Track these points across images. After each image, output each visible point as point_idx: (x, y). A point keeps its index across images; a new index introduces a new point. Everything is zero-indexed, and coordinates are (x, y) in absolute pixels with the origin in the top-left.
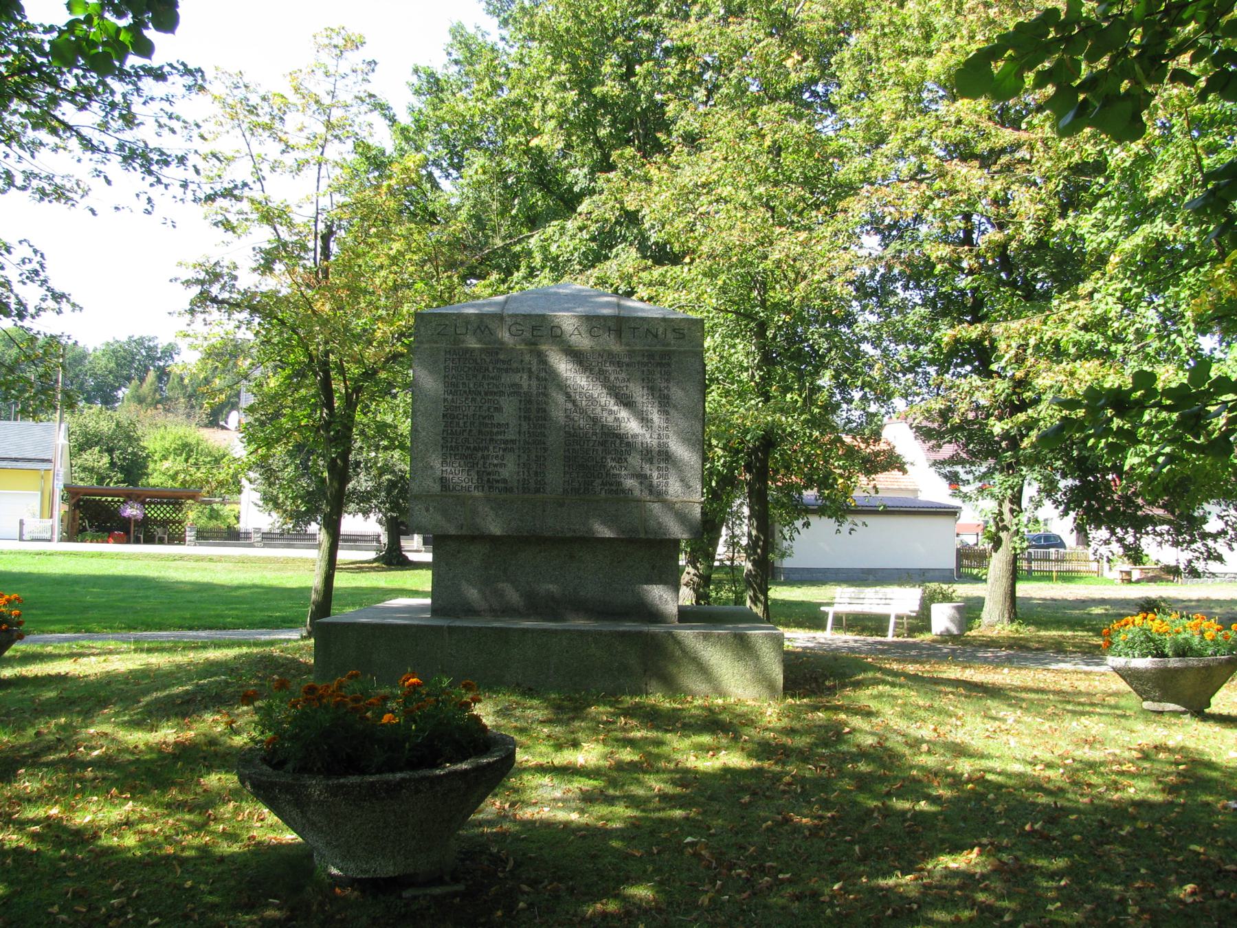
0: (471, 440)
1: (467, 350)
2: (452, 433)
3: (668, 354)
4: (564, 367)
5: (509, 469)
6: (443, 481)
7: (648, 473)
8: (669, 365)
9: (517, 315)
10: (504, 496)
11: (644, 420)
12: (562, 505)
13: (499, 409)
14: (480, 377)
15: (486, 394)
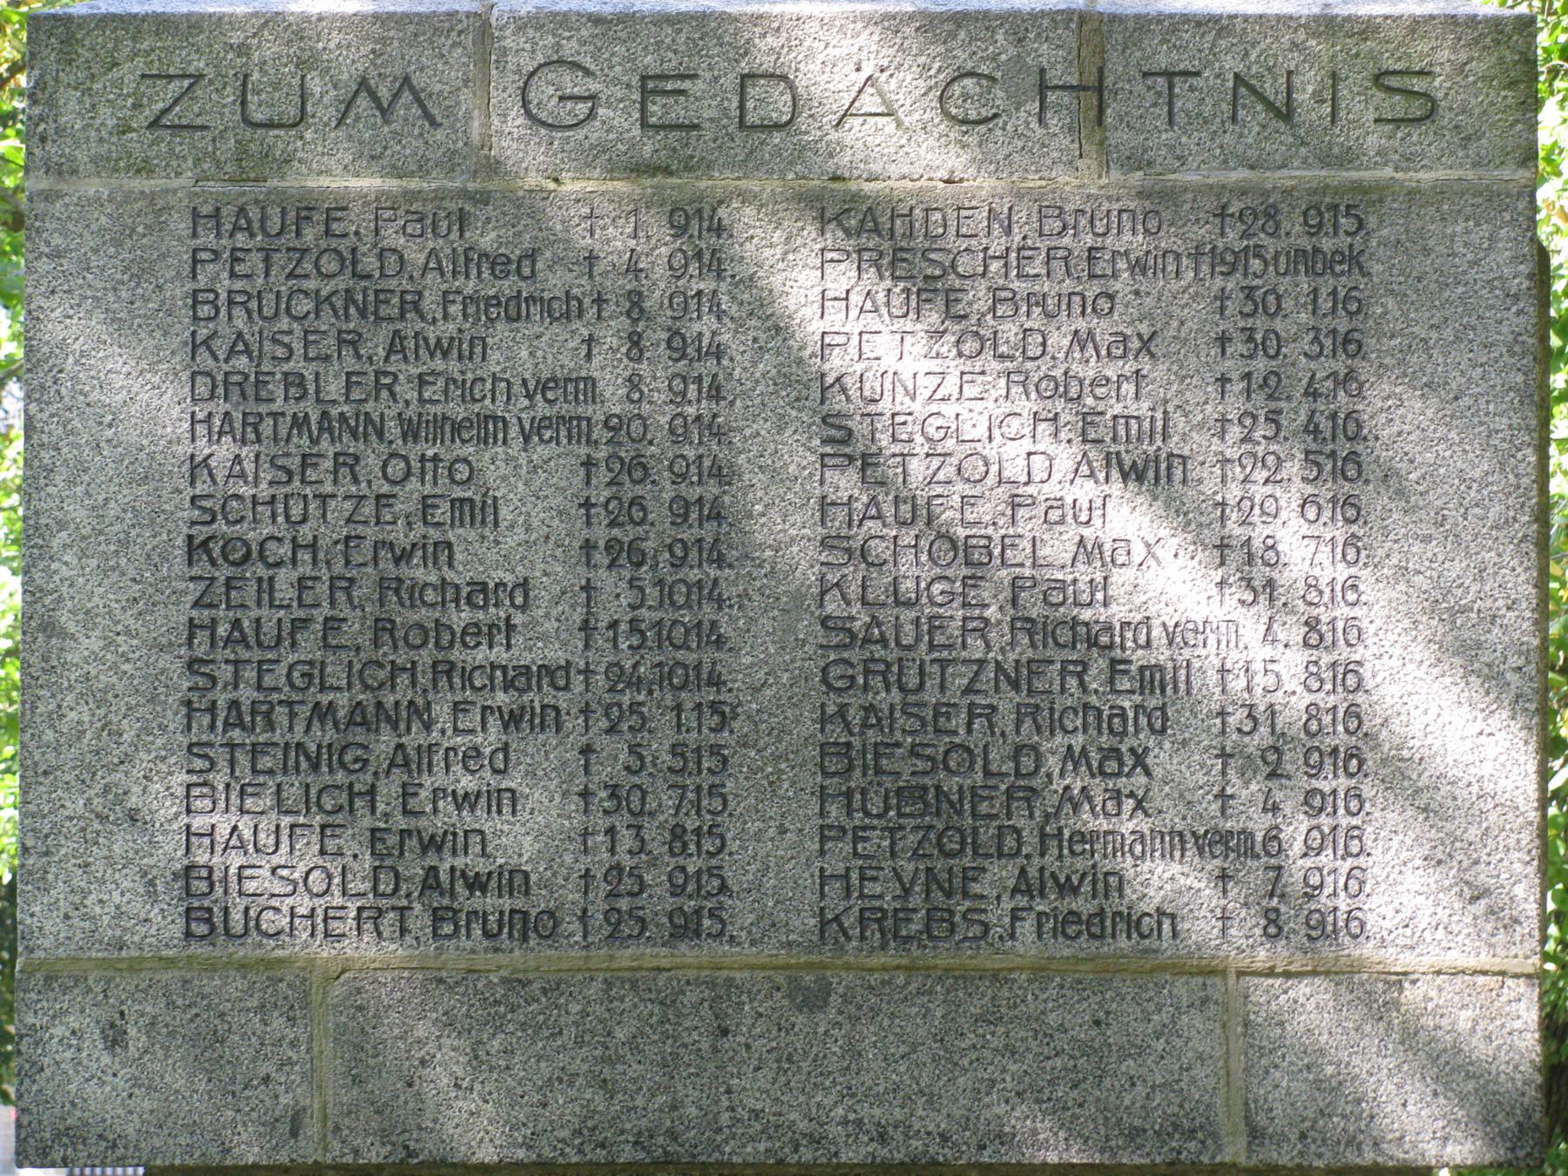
0: (336, 673)
1: (305, 209)
2: (237, 637)
3: (1355, 206)
4: (819, 294)
5: (533, 826)
6: (200, 900)
7: (1260, 825)
8: (1354, 260)
9: (561, 21)
10: (516, 957)
11: (1248, 568)
12: (813, 1000)
13: (477, 511)
14: (376, 343)
15: (411, 432)
